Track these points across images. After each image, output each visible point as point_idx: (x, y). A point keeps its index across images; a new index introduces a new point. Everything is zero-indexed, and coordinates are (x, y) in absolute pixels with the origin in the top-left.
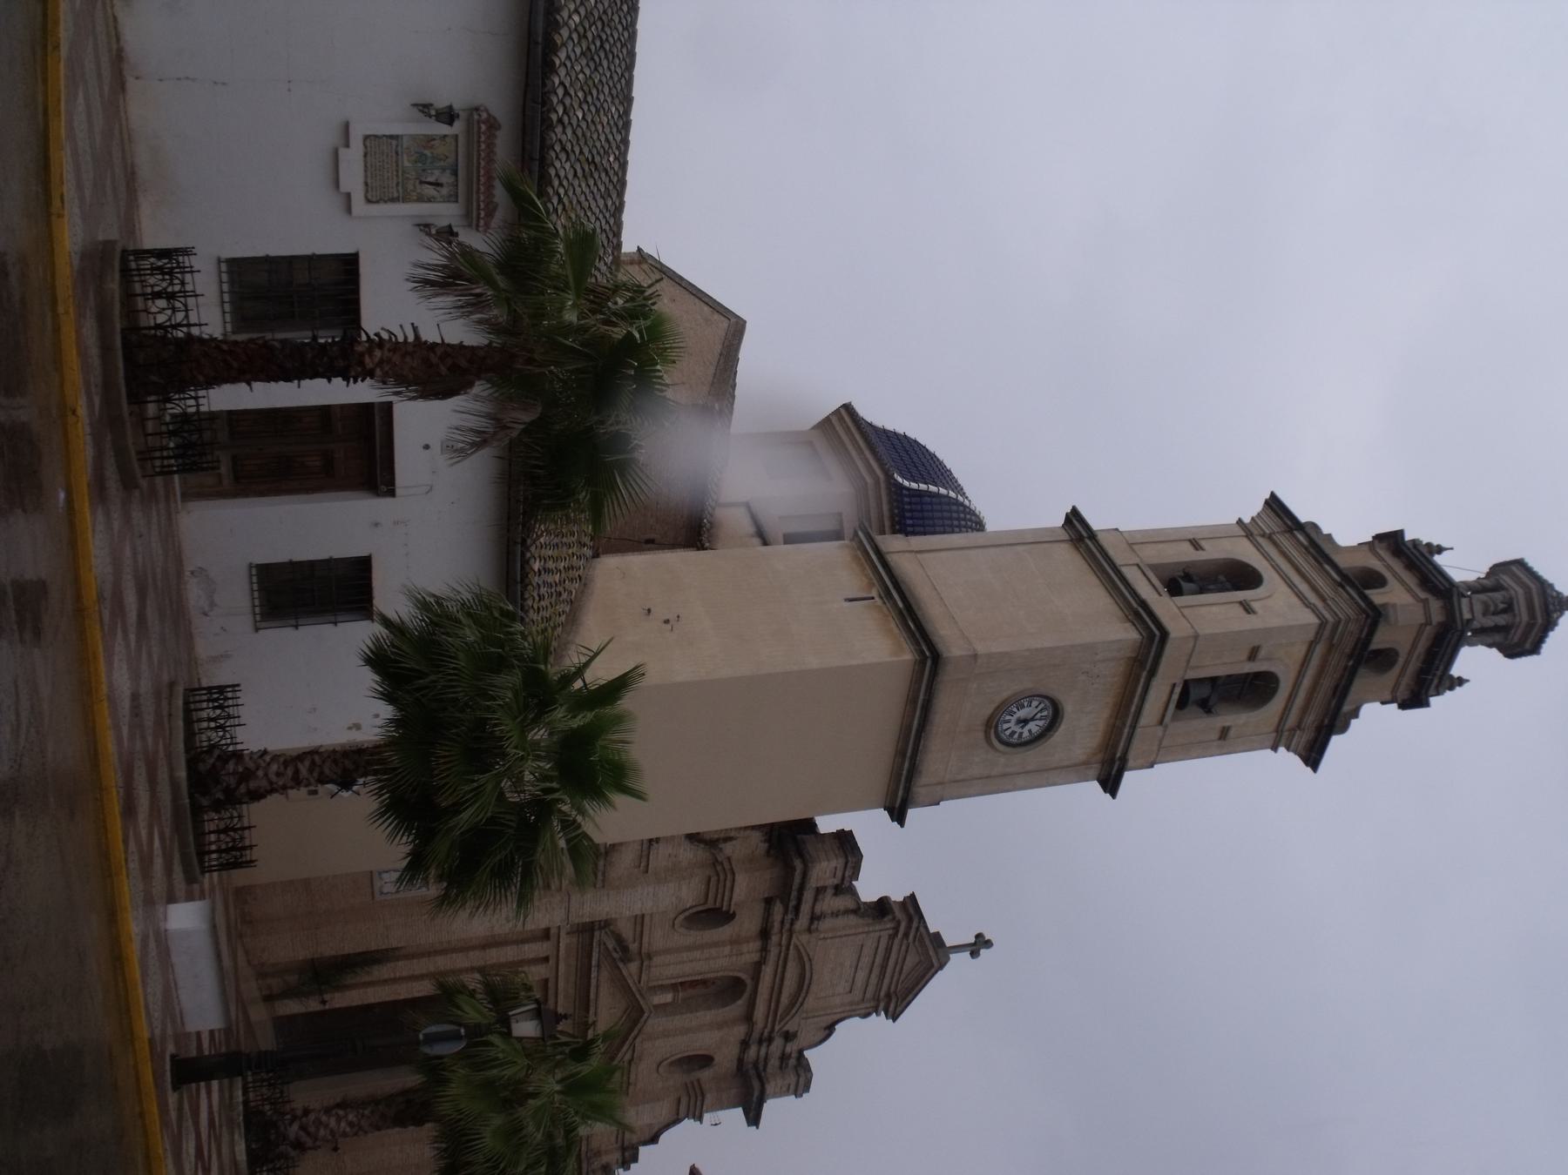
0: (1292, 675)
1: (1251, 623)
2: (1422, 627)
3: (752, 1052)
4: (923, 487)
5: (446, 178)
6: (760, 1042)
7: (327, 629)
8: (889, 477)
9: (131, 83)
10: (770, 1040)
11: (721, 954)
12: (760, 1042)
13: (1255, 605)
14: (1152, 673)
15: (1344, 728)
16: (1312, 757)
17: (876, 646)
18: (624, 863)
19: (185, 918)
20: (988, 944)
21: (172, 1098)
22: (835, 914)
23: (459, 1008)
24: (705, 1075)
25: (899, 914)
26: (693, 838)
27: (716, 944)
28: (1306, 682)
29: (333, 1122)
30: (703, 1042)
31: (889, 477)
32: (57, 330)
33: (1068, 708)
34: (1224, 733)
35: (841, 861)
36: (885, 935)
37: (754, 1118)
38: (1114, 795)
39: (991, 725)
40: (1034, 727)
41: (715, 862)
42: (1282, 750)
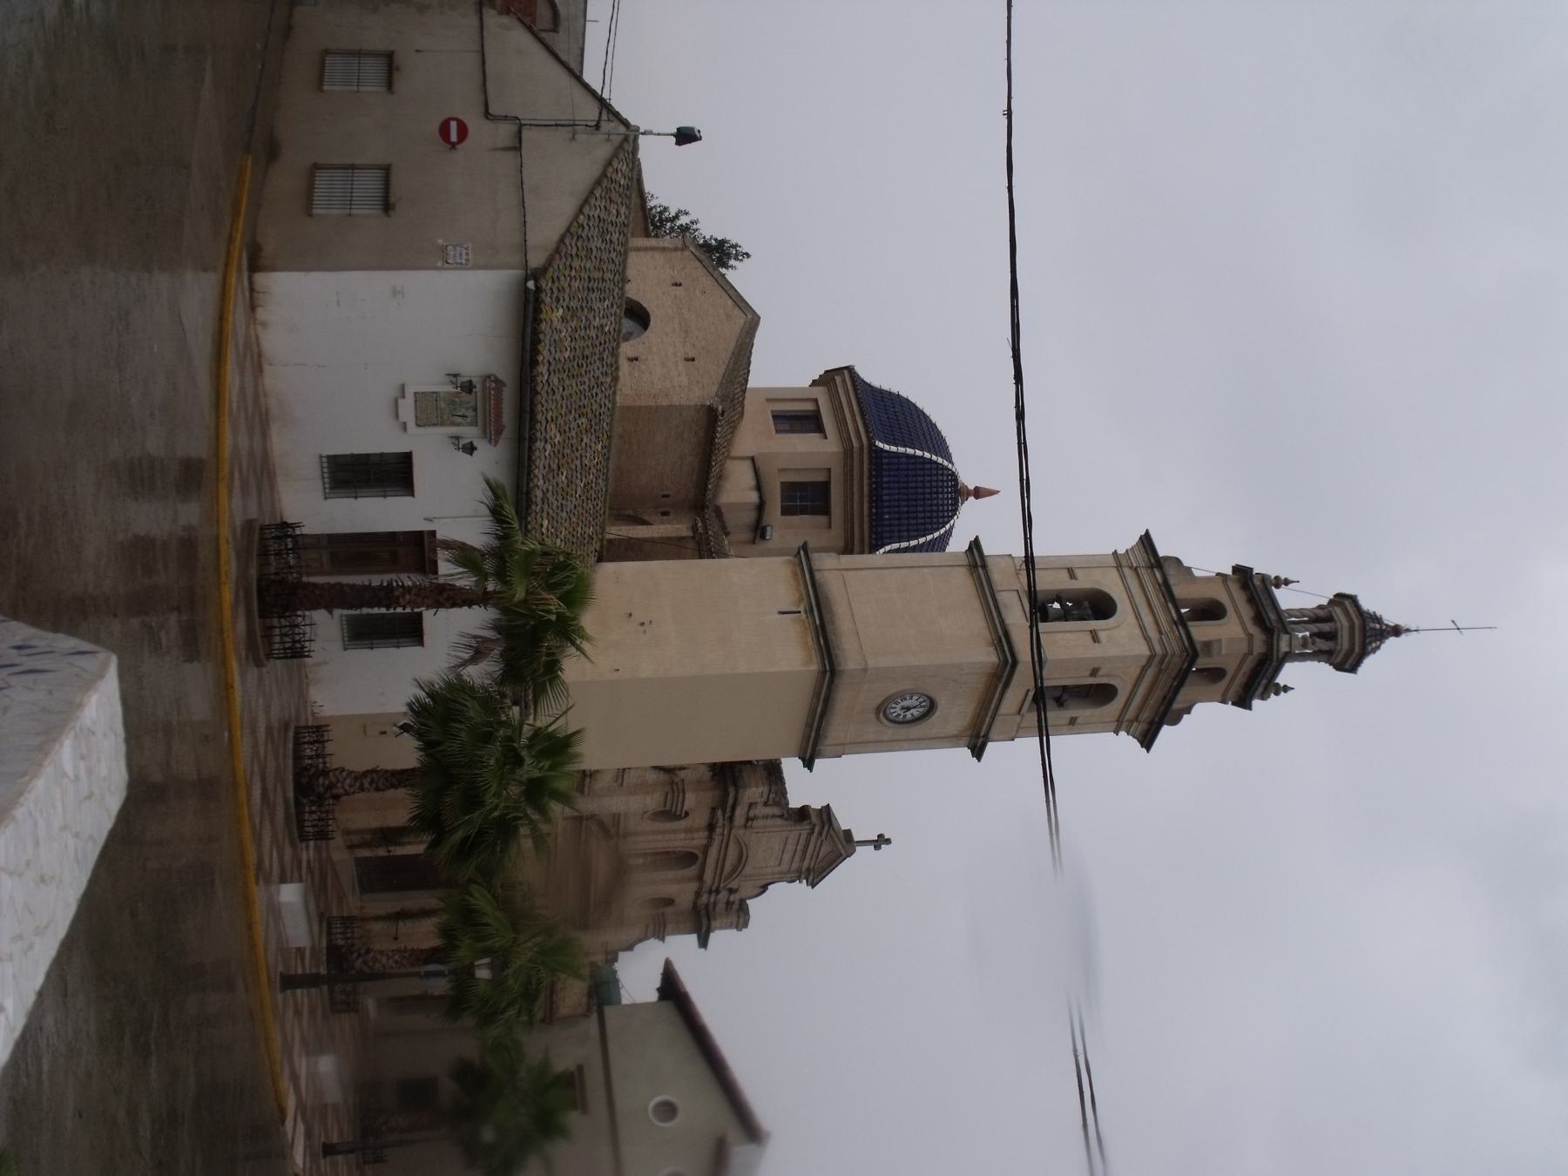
0: (1129, 688)
1: (1097, 651)
2: (1245, 657)
3: (704, 898)
4: (901, 450)
5: (470, 413)
6: (710, 892)
7: (392, 650)
8: (870, 440)
9: (266, 367)
10: (718, 892)
11: (678, 838)
12: (710, 892)
13: (1102, 635)
14: (1007, 685)
15: (1175, 720)
16: (1147, 741)
17: (792, 656)
18: (602, 783)
19: (290, 894)
20: (888, 841)
21: (280, 997)
22: (766, 817)
23: (471, 895)
24: (669, 910)
25: (814, 819)
26: (655, 768)
27: (675, 832)
28: (1142, 690)
29: (384, 960)
30: (669, 890)
31: (871, 444)
32: (224, 646)
33: (942, 702)
34: (1073, 721)
35: (766, 789)
36: (804, 834)
37: (703, 943)
38: (979, 759)
39: (881, 710)
40: (915, 712)
41: (672, 783)
42: (1123, 734)
